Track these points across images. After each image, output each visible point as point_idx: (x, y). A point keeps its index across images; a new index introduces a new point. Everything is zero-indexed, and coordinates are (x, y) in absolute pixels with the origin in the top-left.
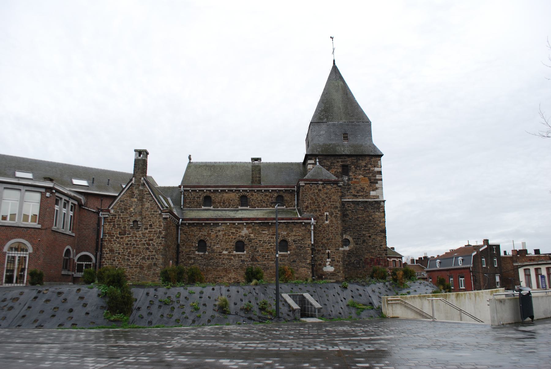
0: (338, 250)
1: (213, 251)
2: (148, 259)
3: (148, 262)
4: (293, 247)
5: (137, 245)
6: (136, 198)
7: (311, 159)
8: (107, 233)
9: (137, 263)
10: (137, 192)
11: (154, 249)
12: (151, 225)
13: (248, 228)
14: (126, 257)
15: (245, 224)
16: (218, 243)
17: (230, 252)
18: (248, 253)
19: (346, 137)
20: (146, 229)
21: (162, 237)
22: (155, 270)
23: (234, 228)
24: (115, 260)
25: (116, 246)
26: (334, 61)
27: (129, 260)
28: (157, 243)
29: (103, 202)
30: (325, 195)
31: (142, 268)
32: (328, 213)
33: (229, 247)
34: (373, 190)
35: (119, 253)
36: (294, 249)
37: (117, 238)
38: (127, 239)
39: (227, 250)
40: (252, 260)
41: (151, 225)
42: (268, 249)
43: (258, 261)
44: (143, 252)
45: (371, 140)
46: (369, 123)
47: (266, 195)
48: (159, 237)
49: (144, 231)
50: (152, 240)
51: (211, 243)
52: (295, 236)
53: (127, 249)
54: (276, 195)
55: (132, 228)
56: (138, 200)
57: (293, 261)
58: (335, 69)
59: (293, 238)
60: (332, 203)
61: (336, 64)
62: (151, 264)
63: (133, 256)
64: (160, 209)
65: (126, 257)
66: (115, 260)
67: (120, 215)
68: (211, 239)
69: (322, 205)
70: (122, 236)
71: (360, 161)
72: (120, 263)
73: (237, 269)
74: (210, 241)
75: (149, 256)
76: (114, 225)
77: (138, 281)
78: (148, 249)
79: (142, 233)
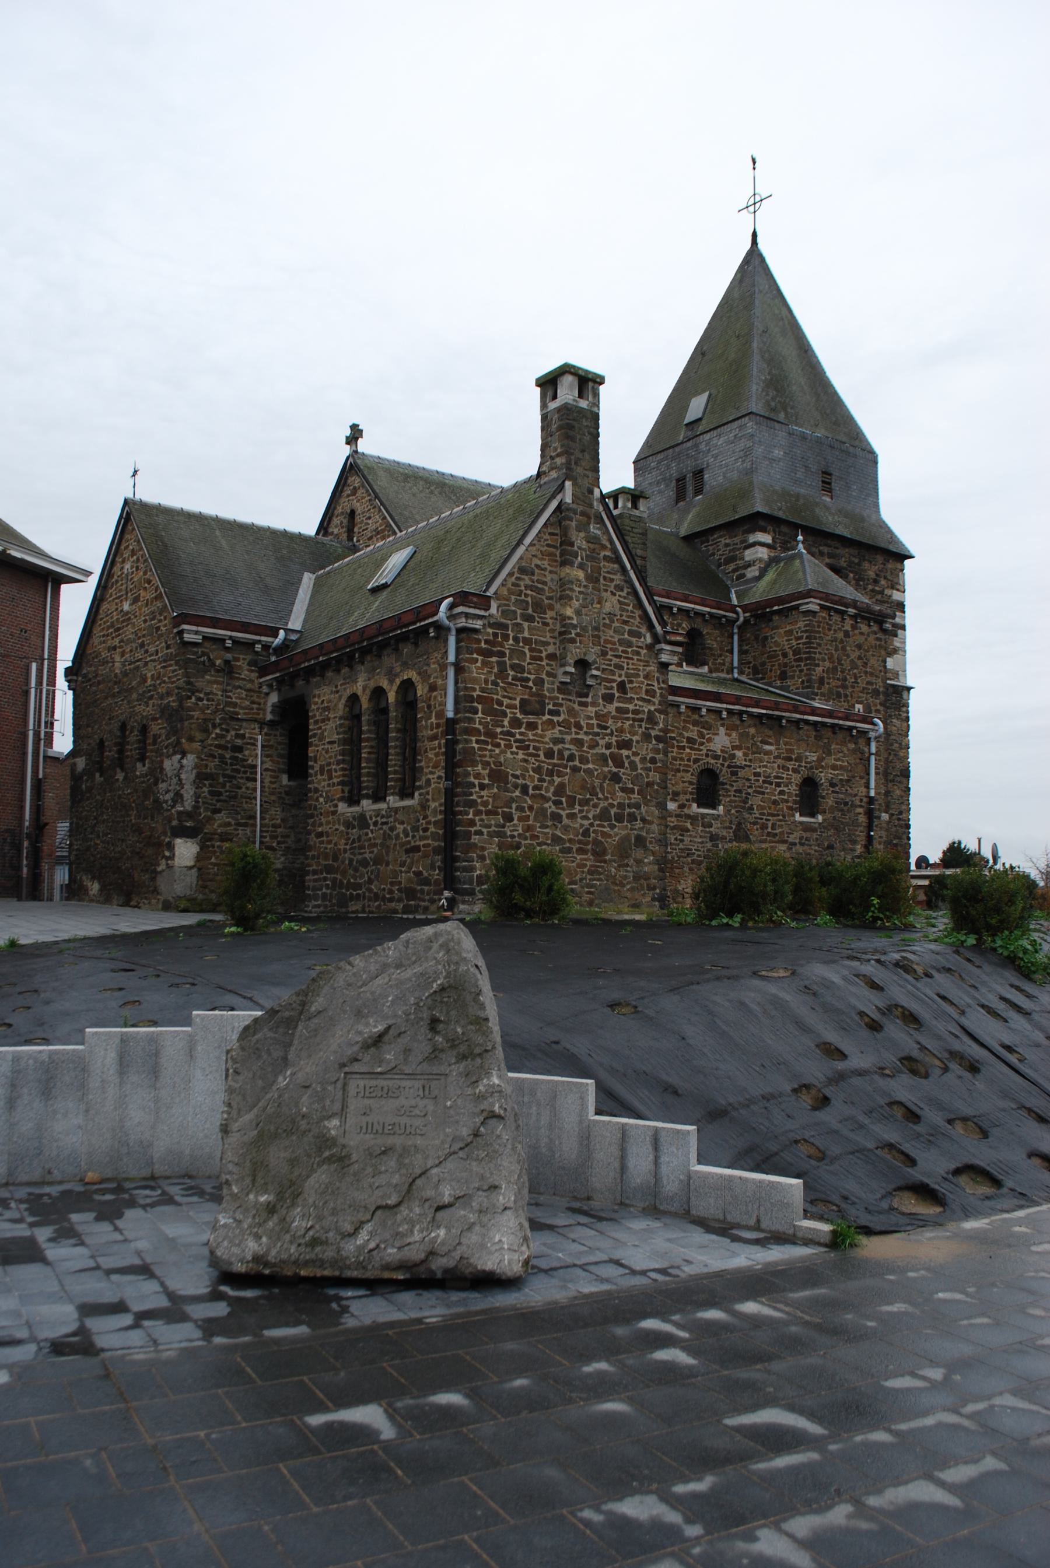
2: (619, 818)
3: (620, 831)
4: (830, 803)
5: (584, 760)
6: (581, 567)
7: (764, 530)
9: (586, 833)
10: (585, 545)
11: (635, 780)
12: (622, 687)
13: (730, 728)
15: (724, 714)
17: (682, 806)
18: (727, 812)
19: (827, 486)
20: (609, 698)
22: (639, 862)
23: (695, 723)
24: (509, 818)
25: (512, 758)
26: (754, 235)
27: (556, 817)
28: (643, 760)
30: (857, 653)
31: (599, 853)
35: (525, 789)
36: (832, 810)
37: (516, 723)
38: (549, 734)
42: (775, 802)
45: (878, 511)
46: (871, 458)
48: (647, 737)
52: (834, 767)
53: (550, 773)
55: (563, 688)
58: (754, 266)
59: (830, 773)
60: (869, 679)
61: (761, 246)
62: (625, 839)
64: (651, 627)
70: (532, 718)
71: (866, 565)
72: (529, 828)
75: (621, 806)
77: (590, 903)
78: (616, 778)
79: (598, 716)
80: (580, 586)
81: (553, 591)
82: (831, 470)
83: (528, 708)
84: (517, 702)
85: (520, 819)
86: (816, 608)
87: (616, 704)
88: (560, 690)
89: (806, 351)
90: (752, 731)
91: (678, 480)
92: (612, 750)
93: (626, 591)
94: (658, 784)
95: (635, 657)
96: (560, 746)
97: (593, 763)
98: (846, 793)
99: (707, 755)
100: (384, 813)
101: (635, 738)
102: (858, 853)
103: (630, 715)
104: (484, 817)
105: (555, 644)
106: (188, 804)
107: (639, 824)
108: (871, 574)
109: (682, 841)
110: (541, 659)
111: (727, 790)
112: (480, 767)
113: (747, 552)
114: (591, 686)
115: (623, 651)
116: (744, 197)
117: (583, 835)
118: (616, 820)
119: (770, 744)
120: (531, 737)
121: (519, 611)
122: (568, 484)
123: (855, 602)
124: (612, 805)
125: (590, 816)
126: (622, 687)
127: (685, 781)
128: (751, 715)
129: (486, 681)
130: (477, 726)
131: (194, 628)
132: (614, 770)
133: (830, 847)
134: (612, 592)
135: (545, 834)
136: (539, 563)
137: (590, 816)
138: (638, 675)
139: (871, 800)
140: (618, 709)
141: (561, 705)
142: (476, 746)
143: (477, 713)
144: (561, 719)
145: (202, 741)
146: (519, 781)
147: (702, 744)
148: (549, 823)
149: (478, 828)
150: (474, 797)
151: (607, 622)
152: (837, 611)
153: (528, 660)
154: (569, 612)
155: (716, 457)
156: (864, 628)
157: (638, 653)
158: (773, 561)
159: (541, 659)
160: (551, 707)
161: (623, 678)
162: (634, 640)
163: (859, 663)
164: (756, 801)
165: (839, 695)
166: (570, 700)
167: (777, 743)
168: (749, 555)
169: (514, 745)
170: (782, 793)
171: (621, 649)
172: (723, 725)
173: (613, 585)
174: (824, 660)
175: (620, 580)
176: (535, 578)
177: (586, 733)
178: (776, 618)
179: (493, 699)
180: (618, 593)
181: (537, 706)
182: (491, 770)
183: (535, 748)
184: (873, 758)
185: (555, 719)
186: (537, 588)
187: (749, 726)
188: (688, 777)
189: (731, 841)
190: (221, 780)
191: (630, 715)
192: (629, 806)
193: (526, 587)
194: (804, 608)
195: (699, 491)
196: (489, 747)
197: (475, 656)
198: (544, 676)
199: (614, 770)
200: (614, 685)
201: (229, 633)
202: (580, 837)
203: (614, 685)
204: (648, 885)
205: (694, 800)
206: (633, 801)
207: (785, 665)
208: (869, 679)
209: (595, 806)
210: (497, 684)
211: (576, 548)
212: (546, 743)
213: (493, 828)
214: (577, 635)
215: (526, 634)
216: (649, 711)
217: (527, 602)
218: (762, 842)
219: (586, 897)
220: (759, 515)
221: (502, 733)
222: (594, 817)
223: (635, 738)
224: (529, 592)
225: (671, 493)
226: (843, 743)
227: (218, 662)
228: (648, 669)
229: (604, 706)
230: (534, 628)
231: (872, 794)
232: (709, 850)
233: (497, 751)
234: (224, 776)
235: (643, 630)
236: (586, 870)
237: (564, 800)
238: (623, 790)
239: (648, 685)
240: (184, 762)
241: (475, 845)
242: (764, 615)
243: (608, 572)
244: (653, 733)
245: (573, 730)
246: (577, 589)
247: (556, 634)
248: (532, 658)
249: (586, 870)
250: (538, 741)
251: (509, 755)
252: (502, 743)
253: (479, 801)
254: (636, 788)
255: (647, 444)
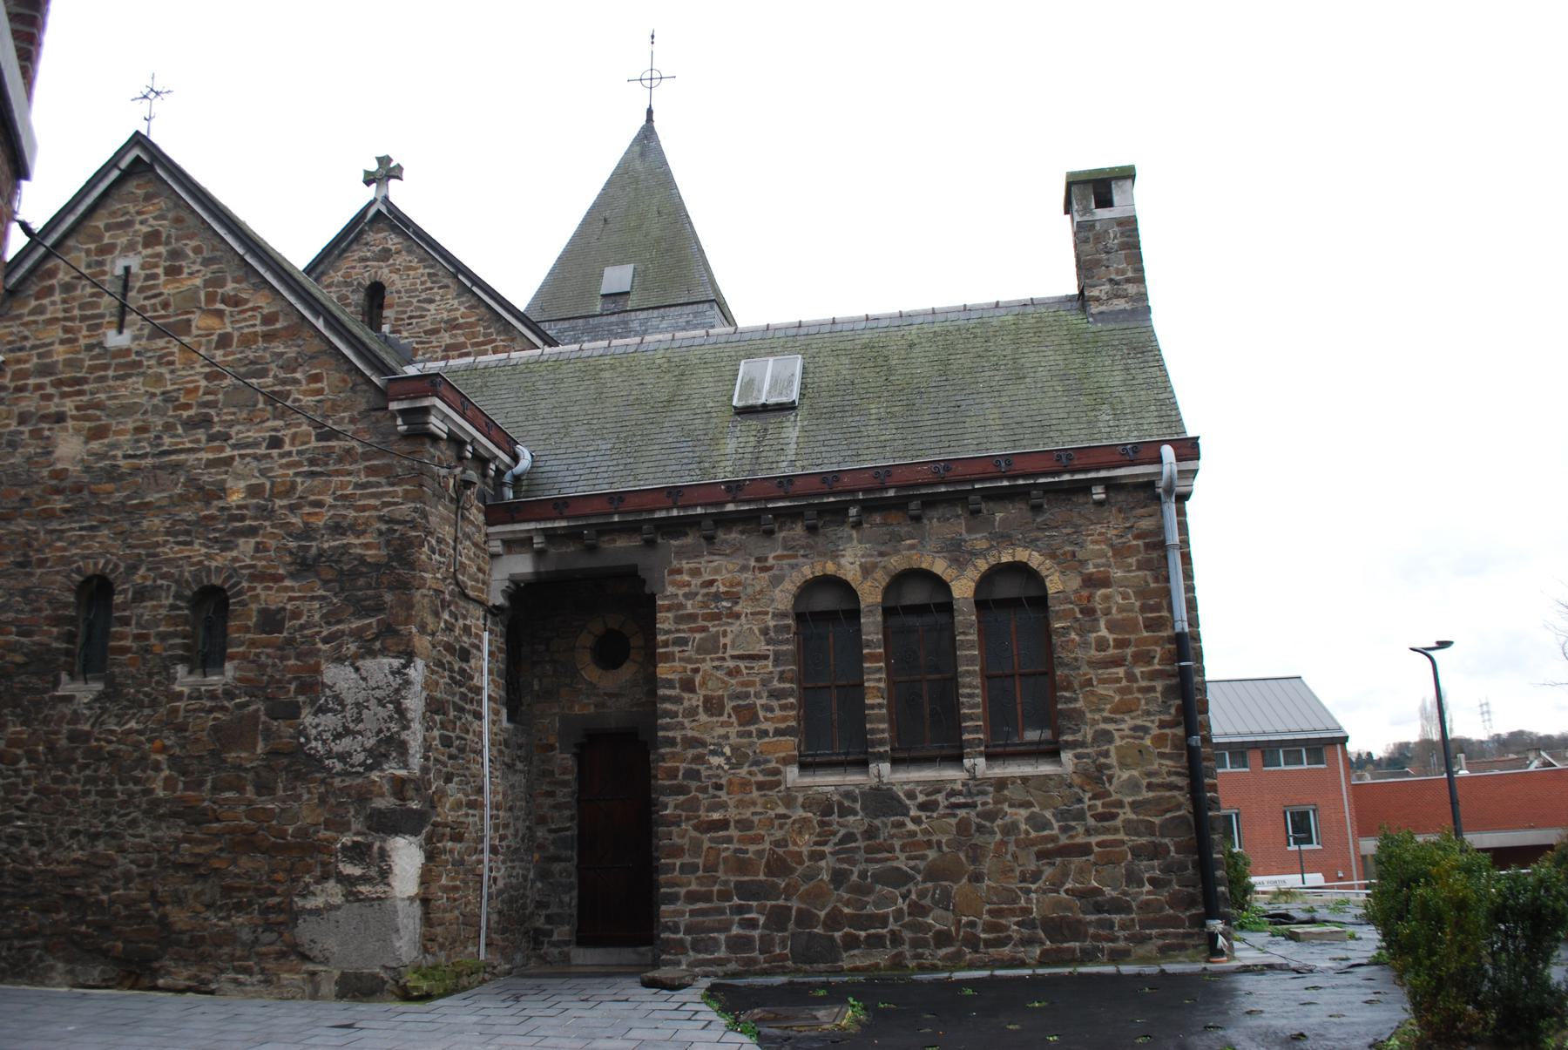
26: (650, 112)
100: (958, 786)
116: (641, 68)
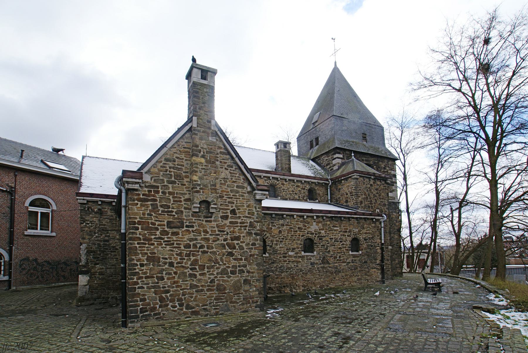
0: (388, 248)
1: (275, 252)
2: (233, 273)
3: (234, 278)
4: (365, 246)
6: (203, 156)
7: (339, 153)
8: (139, 223)
9: (212, 281)
14: (188, 271)
15: (315, 217)
16: (281, 242)
17: (297, 253)
19: (364, 138)
20: (225, 217)
21: (256, 234)
24: (162, 279)
25: (163, 251)
26: (335, 63)
27: (195, 276)
28: (248, 244)
29: (18, 178)
30: (376, 192)
32: (378, 210)
33: (295, 246)
34: (391, 192)
36: (365, 249)
38: (186, 237)
39: (293, 249)
40: (323, 263)
41: (233, 212)
42: (340, 248)
43: (329, 264)
44: (222, 260)
46: (382, 128)
47: (298, 186)
49: (221, 222)
50: (238, 238)
51: (272, 241)
52: (366, 233)
53: (188, 255)
54: (308, 187)
55: (195, 214)
56: (207, 161)
57: (365, 262)
60: (381, 200)
61: (338, 66)
62: (239, 281)
63: (202, 267)
64: (250, 184)
65: (188, 271)
66: (162, 279)
67: (166, 187)
68: (273, 236)
69: (374, 201)
70: (175, 230)
71: (381, 163)
73: (307, 273)
74: (271, 238)
76: (155, 207)
78: (231, 254)
80: (202, 166)
81: (188, 169)
82: (366, 133)
83: (172, 225)
84: (165, 223)
85: (168, 279)
86: (358, 177)
87: (229, 220)
88: (193, 216)
89: (355, 97)
90: (328, 223)
91: (311, 142)
92: (228, 241)
93: (234, 167)
94: (257, 255)
95: (241, 198)
96: (194, 242)
97: (216, 248)
98: (372, 242)
99: (308, 233)
101: (242, 235)
102: (378, 263)
103: (239, 225)
104: (144, 279)
105: (189, 194)
106: (83, 263)
107: (246, 274)
108: (383, 166)
109: (297, 266)
110: (181, 201)
111: (318, 246)
112: (140, 255)
113: (333, 161)
114: (213, 212)
115: (233, 195)
117: (210, 282)
118: (231, 274)
119: (337, 227)
120: (175, 239)
121: (165, 180)
122: (195, 118)
123: (374, 173)
124: (229, 267)
125: (215, 273)
126: (233, 212)
127: (299, 243)
128: (327, 217)
129: (144, 214)
130: (138, 236)
131: (82, 198)
132: (229, 250)
133: (366, 262)
134: (226, 168)
135: (186, 284)
136: (178, 156)
137: (215, 273)
138: (244, 206)
139: (382, 244)
140: (230, 222)
141: (195, 223)
142: (138, 246)
143: (138, 229)
144: (194, 229)
145: (89, 239)
146: (168, 261)
147: (305, 229)
148: (188, 279)
149: (140, 285)
150: (137, 270)
151: (223, 182)
152: (366, 177)
153: (172, 203)
154: (195, 178)
155: (322, 132)
156: (379, 183)
157: (242, 196)
158: (343, 164)
159: (181, 201)
160: (188, 224)
161: (234, 208)
162: (240, 190)
163: (377, 195)
164: (331, 248)
165: (369, 207)
166: (200, 220)
167: (340, 226)
168: (334, 162)
169: (164, 243)
170: (342, 244)
171: (232, 194)
172: (315, 222)
173: (226, 165)
174: (362, 195)
175: (231, 163)
176: (176, 163)
177: (211, 235)
178: (343, 181)
179: (149, 222)
180: (229, 169)
181: (178, 224)
182: (148, 257)
183: (177, 244)
184: (383, 229)
185: (191, 229)
186: (177, 168)
187: (327, 221)
188: (299, 242)
189: (320, 264)
190: (99, 253)
191: (239, 225)
192: (239, 266)
193: (170, 168)
194: (353, 177)
195: (317, 144)
196: (147, 246)
197: (136, 202)
198: (183, 209)
199: (229, 250)
200: (229, 211)
201: (99, 199)
202: (208, 283)
203: (229, 211)
204: (252, 301)
205: (302, 251)
206: (242, 264)
207: (347, 198)
208: (381, 200)
209: (218, 268)
210: (151, 215)
211: (199, 148)
212: (185, 241)
213: (151, 284)
214: (201, 189)
215: (171, 190)
216: (250, 222)
217: (171, 175)
218: (334, 263)
219: (213, 311)
220: (337, 148)
221: (154, 238)
222: (217, 274)
223: (242, 235)
224: (172, 170)
225: (309, 146)
226: (370, 224)
227: (96, 210)
228: (249, 203)
229: (222, 221)
230: (175, 187)
231: (383, 242)
232: (310, 268)
233: (152, 247)
234: (100, 251)
235: (246, 185)
236: (213, 298)
237: (197, 267)
238: (235, 259)
239: (249, 210)
240: (81, 247)
241: (139, 294)
242: (339, 181)
243: (223, 159)
244: (253, 232)
245: (202, 234)
246: (201, 167)
247: (190, 189)
248: (174, 201)
249: (213, 298)
250: (179, 241)
251: (160, 248)
252: (156, 243)
253: (140, 272)
254: (243, 258)
255: (301, 132)
